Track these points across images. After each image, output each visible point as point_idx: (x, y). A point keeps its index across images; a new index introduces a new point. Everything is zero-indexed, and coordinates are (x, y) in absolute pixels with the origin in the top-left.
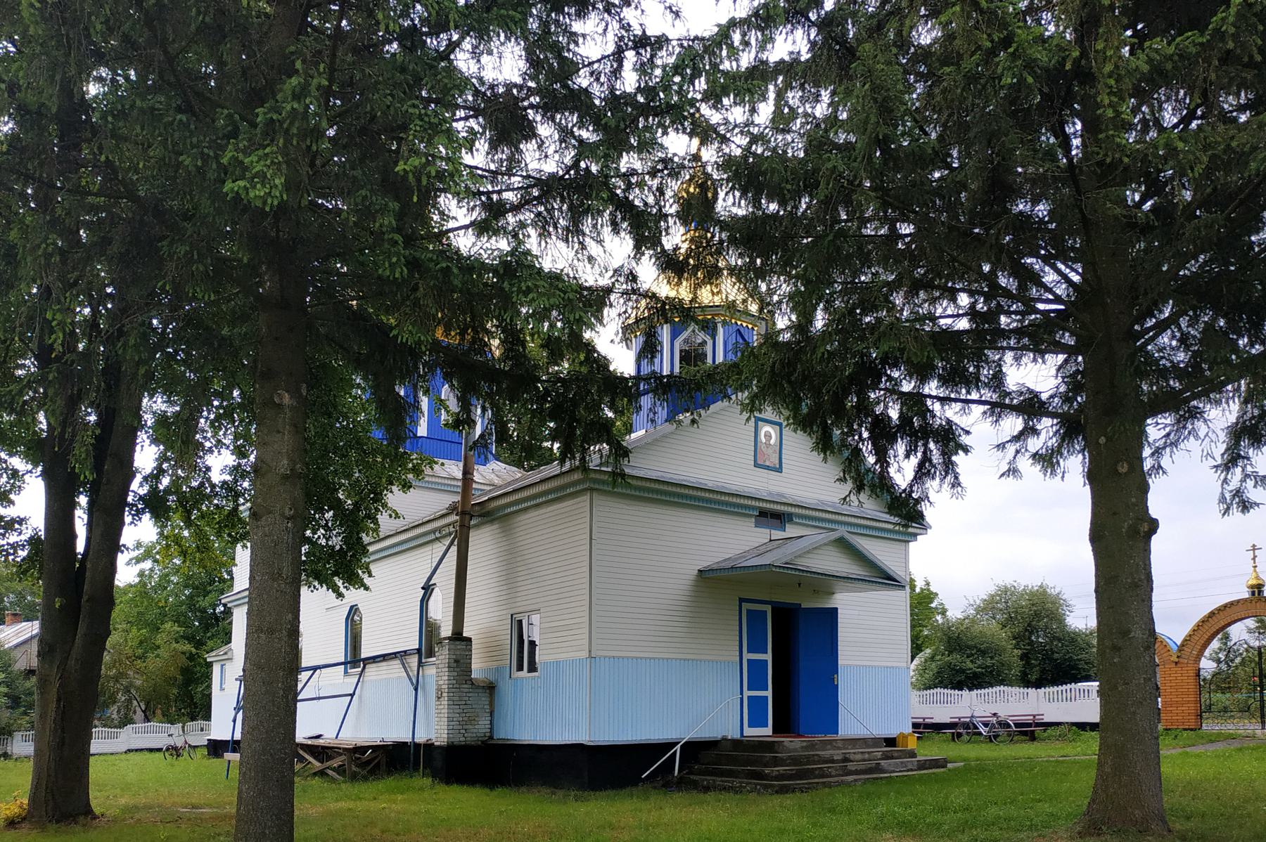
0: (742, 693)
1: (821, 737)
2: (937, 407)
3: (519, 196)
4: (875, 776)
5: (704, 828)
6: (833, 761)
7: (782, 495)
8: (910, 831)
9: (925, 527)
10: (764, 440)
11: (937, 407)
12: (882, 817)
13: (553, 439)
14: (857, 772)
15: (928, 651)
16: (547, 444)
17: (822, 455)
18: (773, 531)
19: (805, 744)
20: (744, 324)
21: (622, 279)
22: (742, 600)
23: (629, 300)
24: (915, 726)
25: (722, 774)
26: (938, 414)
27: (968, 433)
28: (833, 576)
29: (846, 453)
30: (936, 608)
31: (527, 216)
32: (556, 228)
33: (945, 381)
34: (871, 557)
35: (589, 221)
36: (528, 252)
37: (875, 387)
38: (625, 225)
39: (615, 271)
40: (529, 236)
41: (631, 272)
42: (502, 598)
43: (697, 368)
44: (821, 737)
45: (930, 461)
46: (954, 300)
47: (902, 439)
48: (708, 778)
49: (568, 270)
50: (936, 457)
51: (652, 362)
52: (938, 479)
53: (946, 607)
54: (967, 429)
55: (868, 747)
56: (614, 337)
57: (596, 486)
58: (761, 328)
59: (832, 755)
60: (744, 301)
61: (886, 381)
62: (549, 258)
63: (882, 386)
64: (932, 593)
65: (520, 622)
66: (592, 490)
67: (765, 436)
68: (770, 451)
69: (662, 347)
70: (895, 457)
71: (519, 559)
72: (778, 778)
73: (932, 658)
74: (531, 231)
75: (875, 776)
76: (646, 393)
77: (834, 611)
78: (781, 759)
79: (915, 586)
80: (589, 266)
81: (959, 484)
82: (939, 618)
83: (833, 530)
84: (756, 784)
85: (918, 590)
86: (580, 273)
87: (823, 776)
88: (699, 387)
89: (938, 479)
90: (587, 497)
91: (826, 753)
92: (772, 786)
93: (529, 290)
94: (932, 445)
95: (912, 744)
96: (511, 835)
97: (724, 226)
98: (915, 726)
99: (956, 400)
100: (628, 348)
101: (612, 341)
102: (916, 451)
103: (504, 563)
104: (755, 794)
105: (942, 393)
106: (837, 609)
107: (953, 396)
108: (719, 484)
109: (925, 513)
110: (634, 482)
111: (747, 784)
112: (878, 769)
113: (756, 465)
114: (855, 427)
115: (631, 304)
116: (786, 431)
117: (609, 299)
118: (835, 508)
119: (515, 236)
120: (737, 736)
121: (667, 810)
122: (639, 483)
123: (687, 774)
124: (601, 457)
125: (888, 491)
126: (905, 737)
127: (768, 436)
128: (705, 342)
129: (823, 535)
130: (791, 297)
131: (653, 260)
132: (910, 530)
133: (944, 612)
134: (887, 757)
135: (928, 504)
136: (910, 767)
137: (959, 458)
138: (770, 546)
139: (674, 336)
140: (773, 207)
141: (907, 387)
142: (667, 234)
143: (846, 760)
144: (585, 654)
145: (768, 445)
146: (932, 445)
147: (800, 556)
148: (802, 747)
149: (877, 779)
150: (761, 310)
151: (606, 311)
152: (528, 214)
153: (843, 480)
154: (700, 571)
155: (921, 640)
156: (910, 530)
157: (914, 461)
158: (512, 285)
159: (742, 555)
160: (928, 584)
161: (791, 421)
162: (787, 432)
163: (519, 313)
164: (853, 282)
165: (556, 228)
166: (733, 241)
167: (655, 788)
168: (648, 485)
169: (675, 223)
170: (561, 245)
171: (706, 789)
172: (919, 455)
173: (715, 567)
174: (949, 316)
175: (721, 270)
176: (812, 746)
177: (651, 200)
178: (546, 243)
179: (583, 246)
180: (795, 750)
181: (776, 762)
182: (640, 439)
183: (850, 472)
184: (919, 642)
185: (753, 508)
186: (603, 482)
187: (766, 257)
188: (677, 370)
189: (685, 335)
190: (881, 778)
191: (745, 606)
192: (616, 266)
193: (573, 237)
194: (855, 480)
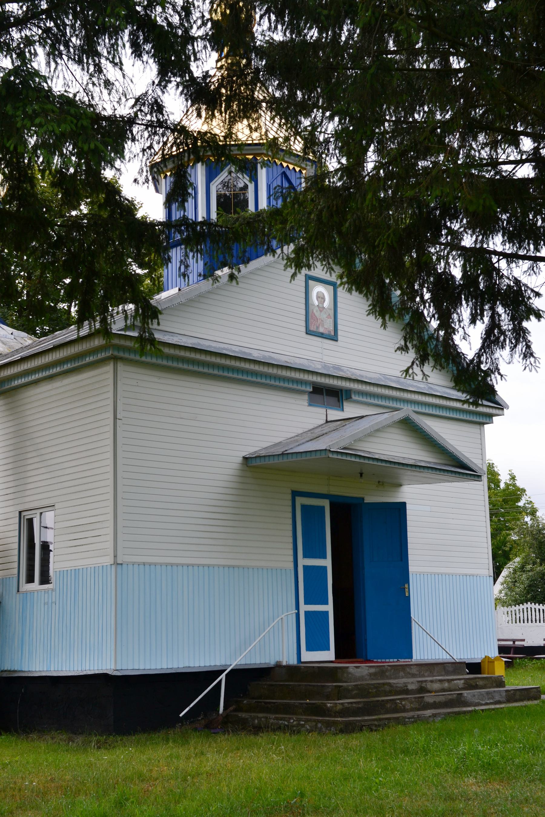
0: (297, 607)
1: (393, 661)
2: (503, 264)
3: (24, 8)
4: (456, 710)
5: (254, 776)
6: (406, 691)
7: (338, 368)
8: (497, 774)
9: (500, 406)
10: (316, 303)
11: (503, 264)
12: (464, 758)
13: (69, 298)
14: (435, 705)
15: (518, 559)
16: (63, 306)
17: (380, 320)
18: (330, 412)
19: (372, 670)
20: (291, 167)
21: (146, 109)
22: (295, 494)
23: (155, 133)
24: (503, 650)
25: (276, 709)
26: (505, 273)
27: (538, 294)
28: (399, 464)
29: (407, 318)
30: (524, 508)
31: (34, 32)
32: (67, 46)
33: (511, 238)
34: (441, 442)
35: (107, 41)
36: (37, 73)
37: (435, 241)
38: (148, 47)
39: (137, 100)
40: (36, 54)
41: (156, 101)
42: (8, 491)
43: (236, 216)
44: (393, 661)
45: (499, 327)
46: (516, 144)
47: (467, 302)
48: (260, 715)
49: (82, 96)
50: (506, 323)
51: (182, 206)
52: (508, 348)
53: (536, 506)
54: (536, 290)
55: (448, 673)
56: (138, 177)
57: (121, 354)
58: (309, 171)
59: (406, 685)
60: (287, 139)
61: (447, 235)
62: (61, 81)
63: (443, 240)
64: (519, 489)
65: (30, 522)
66: (115, 359)
67: (318, 297)
68: (324, 316)
69: (195, 189)
70: (460, 321)
71: (28, 443)
72: (344, 712)
73: (522, 568)
74: (40, 50)
75: (456, 710)
76: (177, 244)
77: (403, 505)
78: (347, 690)
79: (499, 481)
80: (105, 92)
81: (532, 355)
82: (528, 519)
83: (397, 409)
84: (319, 721)
85: (502, 485)
86: (97, 99)
87: (396, 711)
88: (237, 237)
89: (508, 348)
90: (109, 368)
91: (399, 682)
92: (335, 723)
93: (36, 114)
94: (500, 310)
95: (499, 670)
96: (16, 793)
97: (261, 52)
98: (503, 650)
99: (524, 258)
100: (157, 191)
101: (135, 180)
102: (482, 315)
103: (11, 448)
104: (315, 734)
105: (509, 249)
106: (404, 504)
107: (521, 253)
108: (267, 354)
109: (497, 388)
110: (166, 350)
111: (307, 721)
112: (459, 701)
113: (308, 332)
114: (416, 287)
115: (157, 138)
116: (340, 290)
117: (131, 132)
118: (398, 382)
119: (21, 55)
120: (293, 661)
121: (209, 755)
122: (172, 351)
123: (235, 710)
124: (126, 318)
125: (454, 361)
126: (490, 661)
127: (321, 298)
128: (246, 187)
129: (386, 416)
130: (337, 135)
131: (181, 88)
132: (481, 409)
133: (533, 512)
134: (470, 686)
135: (499, 377)
136: (497, 698)
137: (531, 324)
138: (326, 429)
139: (209, 179)
140: (314, 33)
141: (468, 241)
142: (196, 59)
143: (422, 690)
144: (109, 560)
145: (321, 309)
146: (500, 310)
147: (360, 440)
148: (371, 674)
149: (458, 713)
150: (305, 150)
151: (128, 145)
152: (35, 29)
153: (404, 349)
154: (245, 459)
155: (508, 545)
156: (481, 409)
157: (481, 327)
158: (16, 109)
159: (297, 439)
160: (513, 478)
161: (345, 280)
162: (342, 292)
163: (25, 143)
164: (406, 122)
165: (67, 46)
166: (270, 70)
167: (196, 729)
168: (182, 353)
169: (205, 47)
170: (75, 67)
171: (257, 730)
172: (486, 319)
173: (263, 453)
174: (511, 162)
175: (259, 103)
176: (381, 673)
177: (176, 20)
178: (57, 63)
179: (99, 69)
180: (362, 678)
181: (341, 693)
182: (170, 299)
183: (412, 340)
184: (507, 549)
185: (306, 383)
186: (129, 350)
187: (308, 88)
188: (214, 216)
189: (223, 176)
190: (465, 713)
191: (300, 501)
192: (138, 93)
193: (88, 59)
194: (418, 350)
